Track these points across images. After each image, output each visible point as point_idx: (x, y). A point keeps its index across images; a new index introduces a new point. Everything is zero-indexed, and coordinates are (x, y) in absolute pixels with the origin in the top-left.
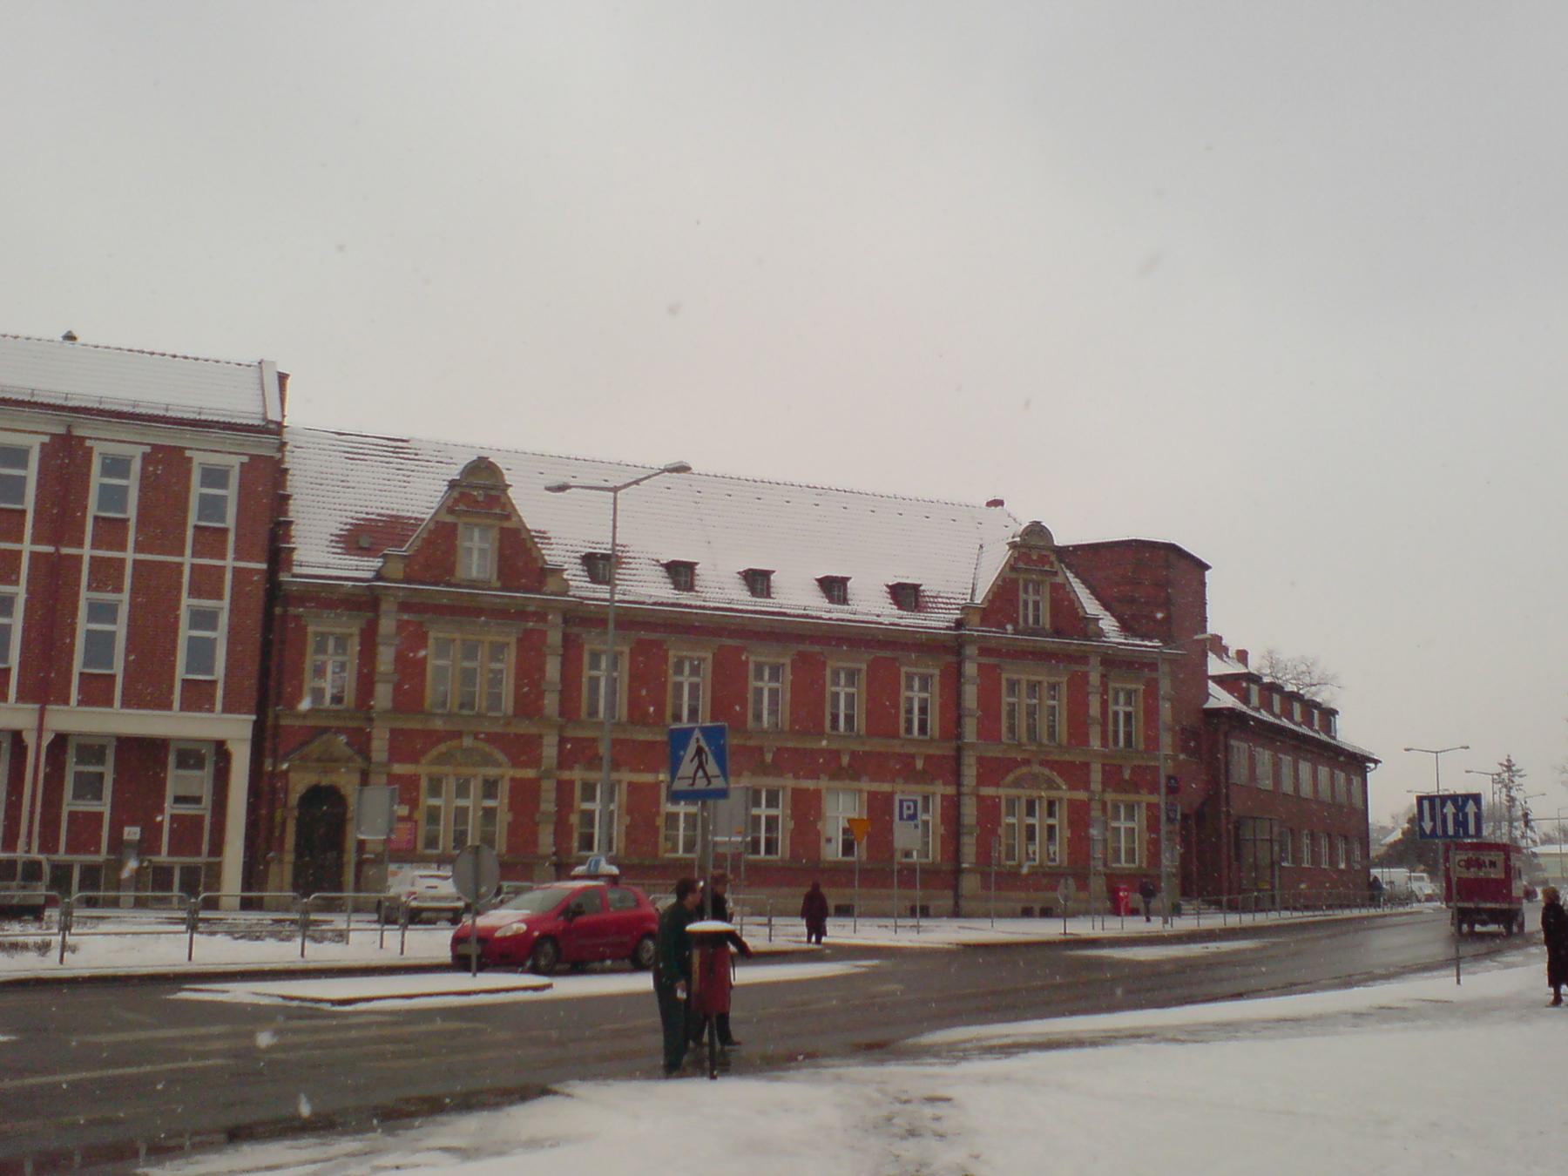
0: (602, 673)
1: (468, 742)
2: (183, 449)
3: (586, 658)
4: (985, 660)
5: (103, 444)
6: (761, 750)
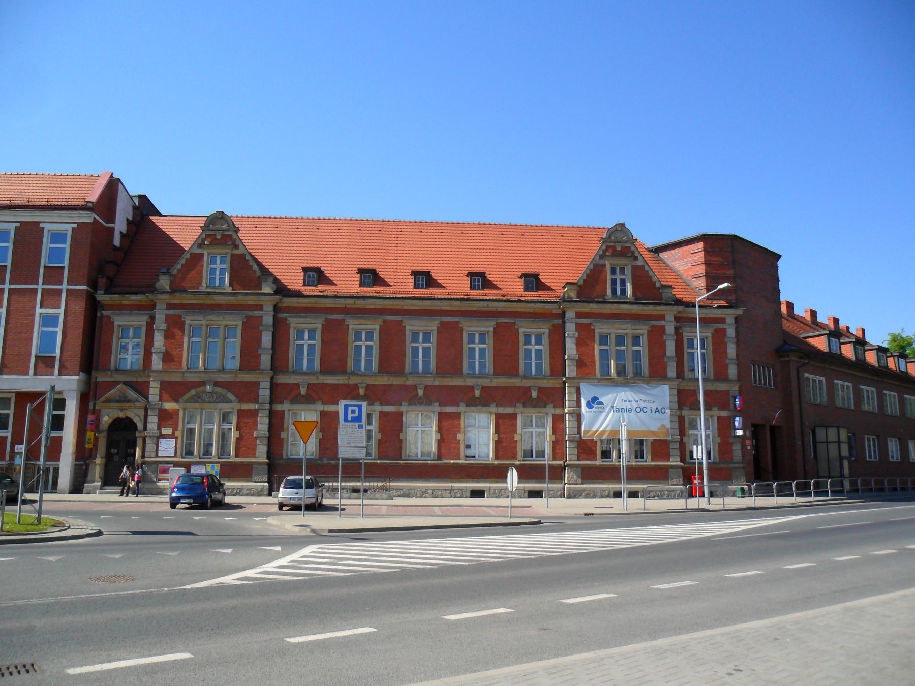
0: (306, 343)
1: (208, 388)
2: (39, 223)
3: (521, 338)
4: (171, 312)
5: (52, 224)
6: (415, 388)
